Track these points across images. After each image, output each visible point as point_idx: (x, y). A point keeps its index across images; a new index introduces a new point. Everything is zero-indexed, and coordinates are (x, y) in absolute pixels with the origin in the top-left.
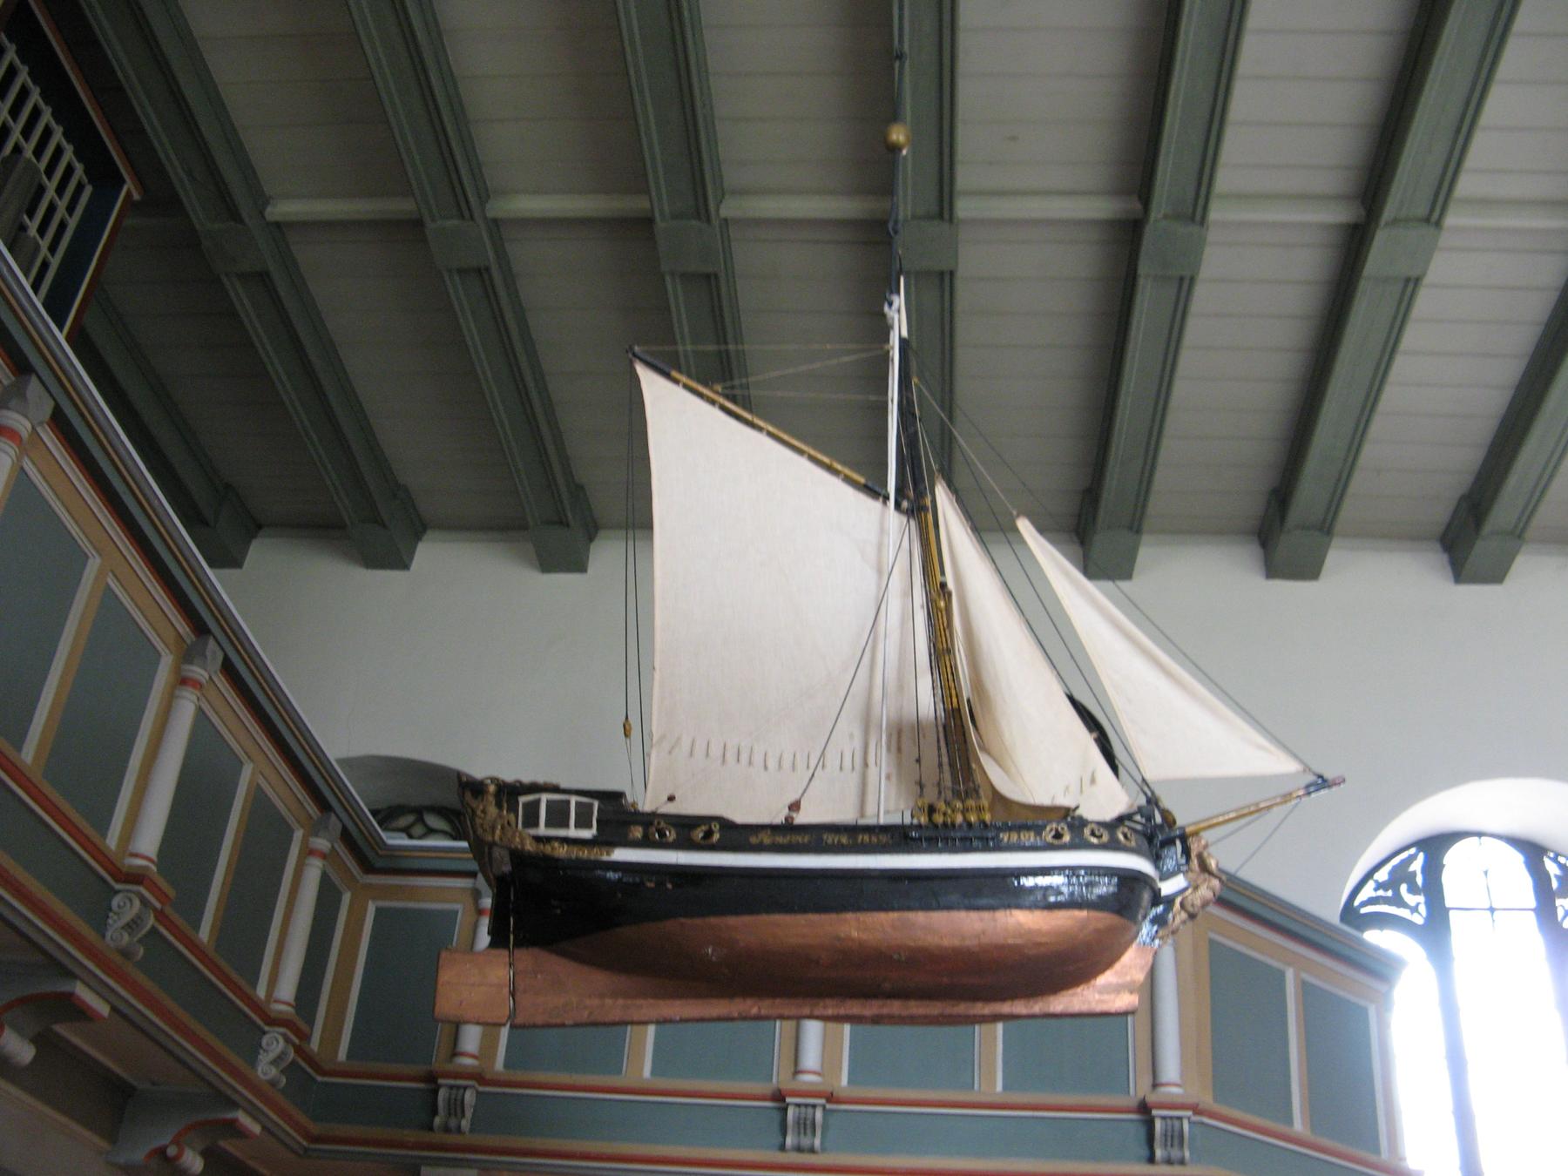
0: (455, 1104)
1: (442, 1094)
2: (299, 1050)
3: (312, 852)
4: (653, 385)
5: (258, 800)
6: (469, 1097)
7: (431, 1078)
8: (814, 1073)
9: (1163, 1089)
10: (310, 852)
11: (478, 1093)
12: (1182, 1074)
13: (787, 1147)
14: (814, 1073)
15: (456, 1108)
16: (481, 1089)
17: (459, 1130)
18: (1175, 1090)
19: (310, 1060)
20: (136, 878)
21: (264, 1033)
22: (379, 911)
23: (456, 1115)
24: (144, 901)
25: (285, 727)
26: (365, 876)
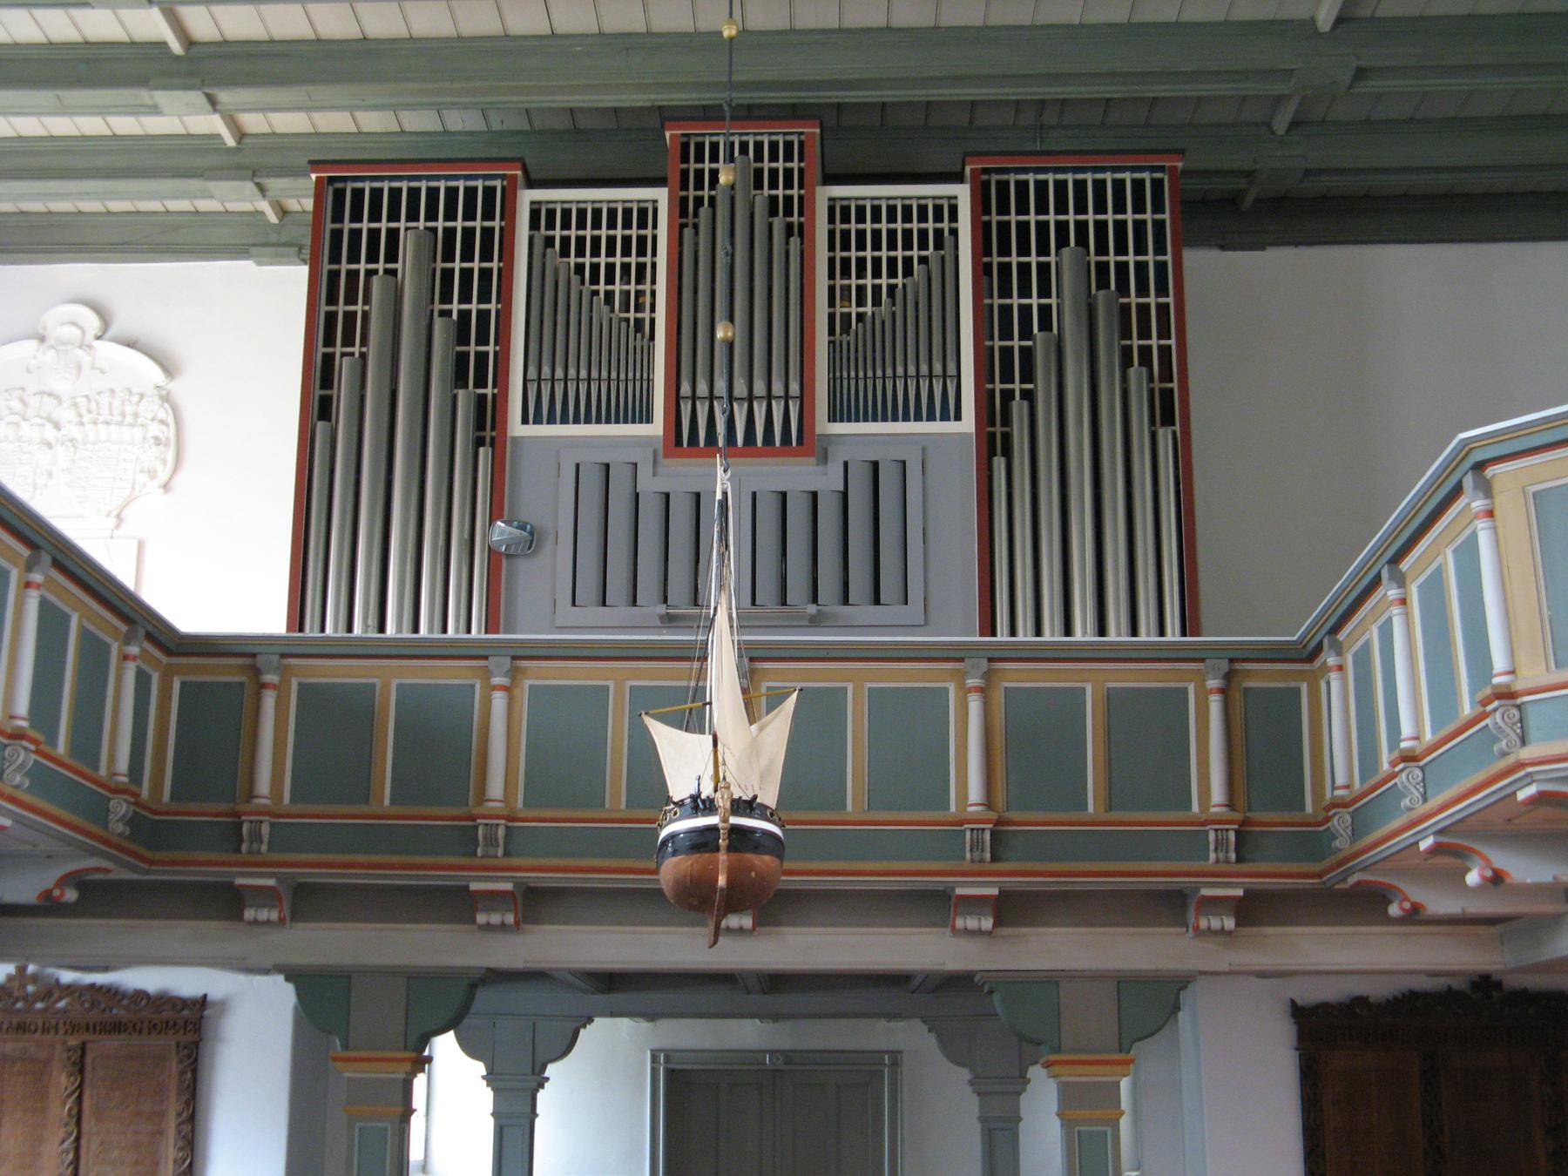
0: (255, 835)
1: (245, 829)
2: (137, 804)
3: (126, 657)
4: (445, 1047)
5: (84, 633)
6: (265, 829)
7: (237, 815)
8: (266, 798)
9: (257, 801)
10: (126, 657)
11: (1349, 813)
12: (1336, 796)
13: (508, 684)
14: (266, 798)
15: (256, 837)
16: (1350, 810)
17: (259, 852)
18: (263, 801)
19: (144, 807)
20: (18, 735)
21: (109, 800)
22: (183, 684)
23: (256, 840)
24: (26, 749)
25: (1383, 557)
26: (1314, 664)
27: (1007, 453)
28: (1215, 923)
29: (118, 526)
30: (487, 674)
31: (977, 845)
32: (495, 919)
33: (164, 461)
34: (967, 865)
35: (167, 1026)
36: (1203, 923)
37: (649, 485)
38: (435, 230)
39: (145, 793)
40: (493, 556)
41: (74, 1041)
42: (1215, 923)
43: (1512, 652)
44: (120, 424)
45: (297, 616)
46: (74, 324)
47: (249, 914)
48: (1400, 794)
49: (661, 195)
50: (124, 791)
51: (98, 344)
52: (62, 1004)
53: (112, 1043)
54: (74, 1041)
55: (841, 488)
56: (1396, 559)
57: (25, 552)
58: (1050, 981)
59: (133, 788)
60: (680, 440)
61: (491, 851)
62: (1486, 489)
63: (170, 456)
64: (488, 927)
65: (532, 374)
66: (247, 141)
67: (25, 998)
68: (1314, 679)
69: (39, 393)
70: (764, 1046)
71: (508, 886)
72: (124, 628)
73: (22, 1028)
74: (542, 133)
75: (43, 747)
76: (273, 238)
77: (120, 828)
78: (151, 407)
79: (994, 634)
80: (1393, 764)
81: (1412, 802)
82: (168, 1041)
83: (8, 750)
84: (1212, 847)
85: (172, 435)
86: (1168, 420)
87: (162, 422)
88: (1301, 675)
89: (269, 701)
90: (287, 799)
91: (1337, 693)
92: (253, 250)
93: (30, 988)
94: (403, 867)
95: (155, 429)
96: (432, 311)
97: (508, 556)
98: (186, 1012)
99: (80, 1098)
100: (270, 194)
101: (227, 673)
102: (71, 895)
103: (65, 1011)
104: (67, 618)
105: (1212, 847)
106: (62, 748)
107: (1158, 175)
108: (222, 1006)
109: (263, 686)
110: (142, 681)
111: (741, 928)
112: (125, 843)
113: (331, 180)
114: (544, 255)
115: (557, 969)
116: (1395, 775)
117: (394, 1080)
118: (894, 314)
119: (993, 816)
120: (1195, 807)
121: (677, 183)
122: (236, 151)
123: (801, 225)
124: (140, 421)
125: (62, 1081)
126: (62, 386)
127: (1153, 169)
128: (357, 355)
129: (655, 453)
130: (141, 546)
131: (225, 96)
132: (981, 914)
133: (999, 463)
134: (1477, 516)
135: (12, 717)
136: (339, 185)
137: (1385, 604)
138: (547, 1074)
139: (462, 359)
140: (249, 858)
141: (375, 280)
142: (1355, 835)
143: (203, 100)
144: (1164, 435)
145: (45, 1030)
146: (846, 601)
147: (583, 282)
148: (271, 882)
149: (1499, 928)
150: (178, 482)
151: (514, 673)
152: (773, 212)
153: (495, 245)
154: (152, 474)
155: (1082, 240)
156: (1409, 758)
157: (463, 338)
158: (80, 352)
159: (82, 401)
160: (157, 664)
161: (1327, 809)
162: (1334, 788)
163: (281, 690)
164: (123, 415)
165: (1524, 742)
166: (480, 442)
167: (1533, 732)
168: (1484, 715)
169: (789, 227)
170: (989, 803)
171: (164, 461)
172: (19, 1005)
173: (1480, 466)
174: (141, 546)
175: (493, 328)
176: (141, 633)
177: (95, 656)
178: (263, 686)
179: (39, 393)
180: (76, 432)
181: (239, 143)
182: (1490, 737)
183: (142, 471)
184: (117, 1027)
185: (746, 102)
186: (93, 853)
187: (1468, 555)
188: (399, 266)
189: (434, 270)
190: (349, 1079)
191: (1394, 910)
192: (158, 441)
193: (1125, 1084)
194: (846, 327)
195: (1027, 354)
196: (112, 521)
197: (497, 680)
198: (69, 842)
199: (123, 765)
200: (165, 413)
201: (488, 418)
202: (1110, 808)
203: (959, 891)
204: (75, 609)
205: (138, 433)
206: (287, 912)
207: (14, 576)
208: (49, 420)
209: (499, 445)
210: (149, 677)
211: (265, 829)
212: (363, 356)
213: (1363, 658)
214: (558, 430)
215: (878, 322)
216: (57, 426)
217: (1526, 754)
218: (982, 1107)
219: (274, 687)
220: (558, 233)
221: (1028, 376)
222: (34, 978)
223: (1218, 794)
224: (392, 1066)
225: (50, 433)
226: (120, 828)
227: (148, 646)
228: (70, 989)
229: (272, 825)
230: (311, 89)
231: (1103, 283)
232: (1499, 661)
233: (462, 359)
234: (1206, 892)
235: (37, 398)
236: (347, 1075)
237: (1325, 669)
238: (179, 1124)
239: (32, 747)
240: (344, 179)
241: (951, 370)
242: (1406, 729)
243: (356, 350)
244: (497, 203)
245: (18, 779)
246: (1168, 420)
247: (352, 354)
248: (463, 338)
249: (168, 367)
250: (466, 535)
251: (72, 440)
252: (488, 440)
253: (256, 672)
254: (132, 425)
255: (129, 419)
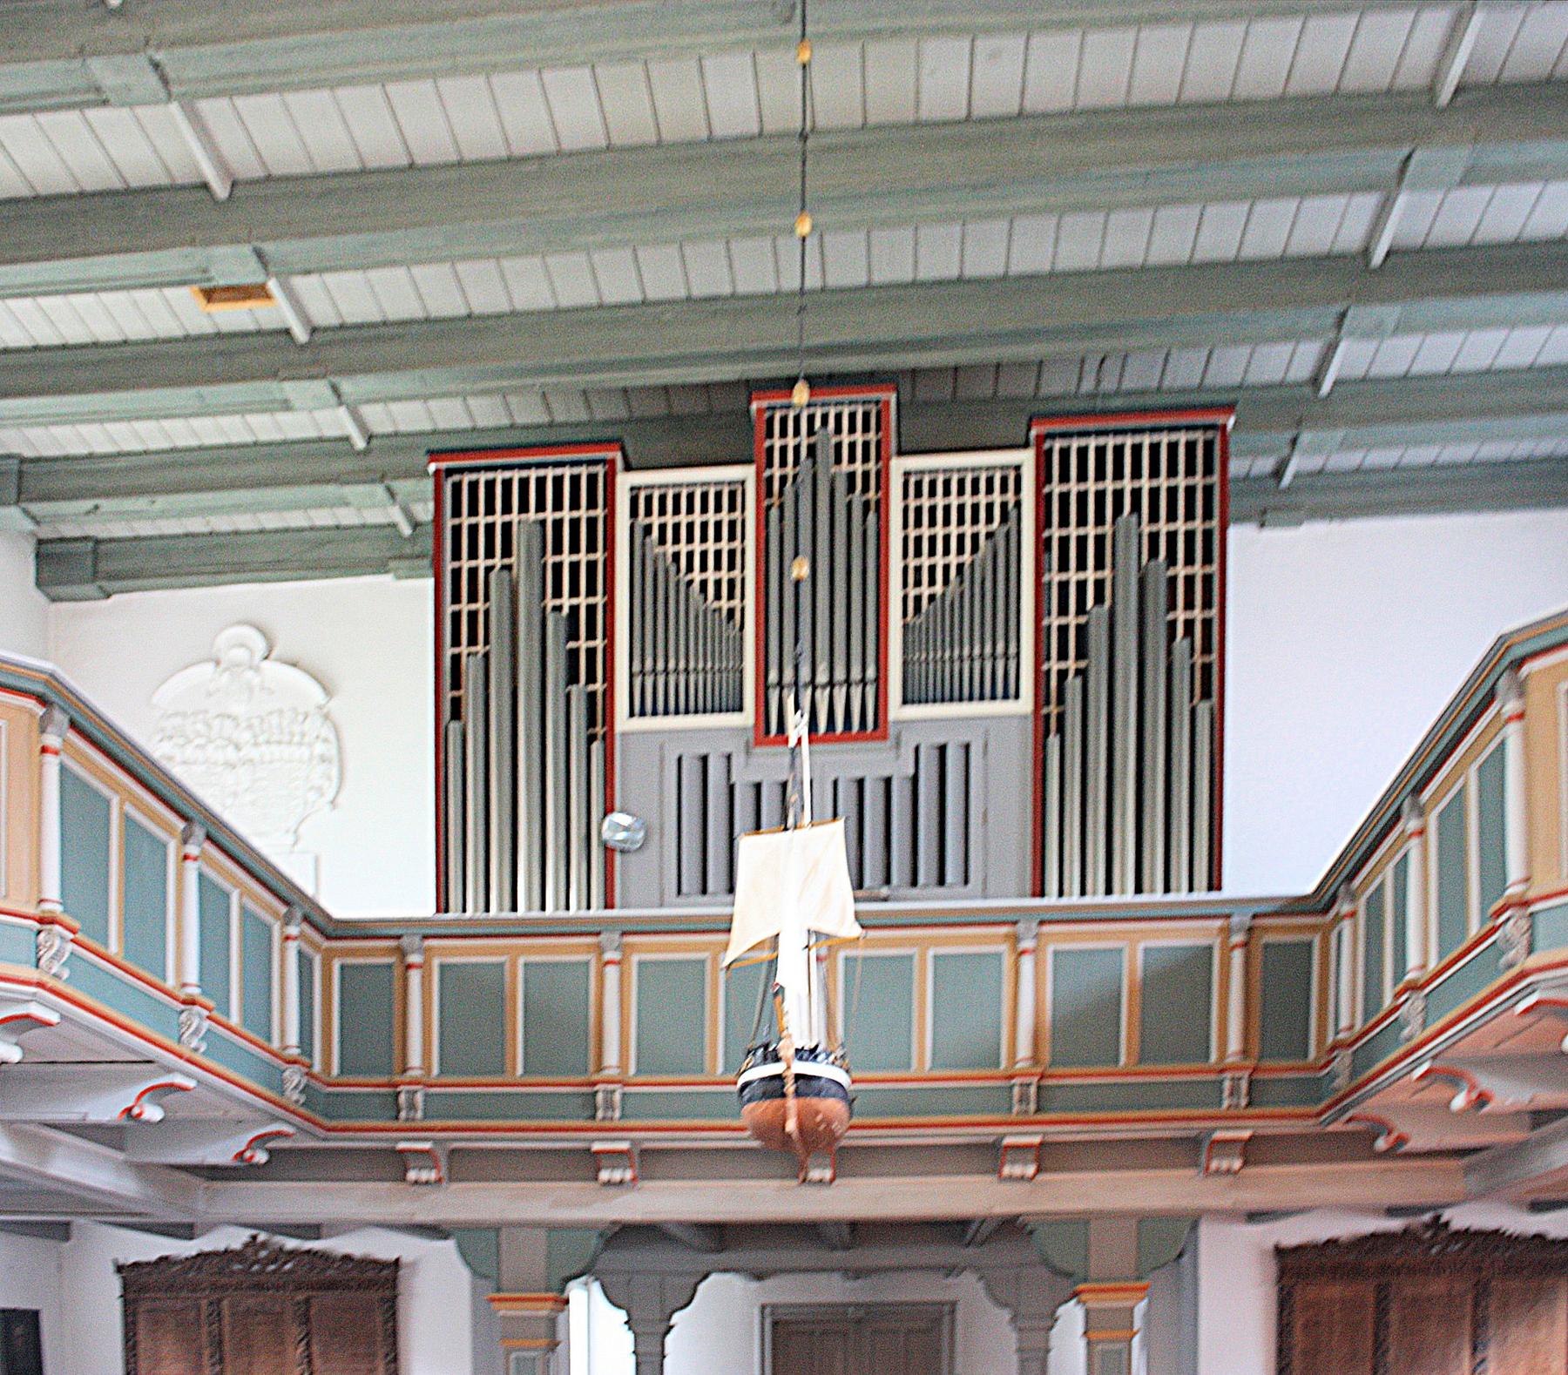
5: (243, 910)
6: (419, 1098)
24: (200, 1015)
27: (1061, 730)
28: (1224, 1164)
29: (295, 843)
30: (600, 950)
31: (1024, 1099)
32: (617, 1175)
33: (329, 778)
34: (1013, 1117)
35: (370, 1284)
36: (1214, 1165)
37: (743, 778)
38: (543, 523)
39: (317, 1068)
40: (608, 851)
41: (300, 1297)
42: (1224, 1164)
43: (1529, 861)
44: (290, 743)
45: (443, 905)
46: (242, 645)
47: (412, 1175)
48: (1399, 1025)
49: (747, 473)
50: (295, 1062)
51: (266, 664)
52: (288, 1266)
53: (330, 1297)
54: (300, 1297)
55: (911, 771)
56: (1418, 789)
57: (181, 825)
58: (1082, 1220)
59: (306, 1060)
60: (769, 731)
61: (609, 1114)
62: (1521, 691)
63: (334, 772)
64: (609, 1183)
65: (637, 667)
66: (374, 442)
67: (257, 1262)
68: (1325, 931)
69: (218, 716)
70: (845, 1300)
71: (624, 1146)
72: (283, 909)
73: (259, 1287)
74: (641, 420)
75: (215, 1014)
76: (408, 550)
77: (295, 1096)
78: (315, 726)
79: (1042, 894)
80: (1397, 996)
81: (1413, 1030)
82: (375, 1295)
83: (184, 1015)
84: (1226, 1093)
85: (334, 751)
86: (1206, 695)
87: (326, 740)
88: (1313, 928)
89: (415, 977)
90: (435, 1070)
91: (1350, 938)
92: (392, 564)
93: (263, 1254)
94: (536, 1130)
95: (319, 748)
96: (544, 608)
97: (623, 852)
98: (385, 1272)
99: (308, 1345)
100: (399, 498)
101: (375, 955)
102: (261, 1157)
103: (290, 1272)
104: (227, 896)
105: (1226, 1093)
106: (235, 1020)
107: (1210, 435)
108: (413, 1265)
109: (409, 967)
110: (304, 962)
111: (821, 1181)
112: (302, 1110)
113: (450, 472)
114: (643, 545)
115: (666, 1222)
116: (1397, 1008)
117: (537, 1318)
118: (962, 595)
119: (1039, 1070)
120: (1214, 1057)
121: (764, 461)
122: (366, 452)
123: (878, 502)
124: (306, 740)
125: (295, 1331)
126: (238, 709)
127: (1206, 428)
128: (480, 655)
129: (747, 743)
130: (317, 860)
131: (346, 386)
132: (1025, 1163)
133: (1053, 741)
134: (1510, 719)
135: (184, 985)
136: (456, 478)
137: (1405, 837)
138: (672, 1322)
139: (573, 655)
140: (408, 1125)
141: (493, 575)
142: (1354, 1073)
143: (328, 392)
144: (1203, 709)
145: (278, 1288)
146: (914, 883)
147: (678, 571)
148: (427, 1146)
149: (1466, 1160)
150: (340, 799)
151: (625, 949)
152: (851, 488)
153: (600, 535)
154: (320, 791)
155: (1136, 507)
156: (1414, 987)
157: (573, 635)
158: (249, 674)
159: (256, 722)
160: (317, 948)
161: (1333, 1049)
162: (1337, 1033)
163: (424, 967)
164: (292, 734)
165: (1530, 950)
166: (591, 739)
167: (1540, 942)
168: (1494, 930)
169: (866, 505)
170: (1035, 1058)
171: (329, 778)
172: (256, 1267)
173: (1519, 663)
174: (317, 860)
175: (599, 621)
176: (299, 914)
177: (258, 938)
178: (409, 967)
179: (218, 716)
180: (255, 753)
181: (368, 443)
182: (1498, 950)
183: (312, 788)
184: (331, 1285)
185: (827, 371)
186: (275, 1119)
187: (1495, 767)
188: (513, 560)
189: (544, 566)
190: (503, 1317)
191: (1381, 1144)
192: (323, 759)
193: (1140, 1308)
194: (918, 609)
195: (1082, 630)
196: (290, 838)
197: (608, 956)
198: (257, 1109)
199: (293, 1038)
200: (327, 732)
201: (599, 712)
202: (1141, 1061)
203: (1008, 1141)
204: (236, 886)
205: (305, 751)
206: (444, 1172)
207: (172, 846)
208: (230, 740)
209: (608, 739)
210: (311, 962)
211: (419, 1098)
212: (486, 656)
213: (1376, 901)
214: (661, 722)
215: (948, 603)
216: (238, 747)
217: (1532, 962)
218: (1020, 1340)
219: (420, 966)
220: (656, 520)
221: (1082, 653)
222: (264, 1245)
223: (1234, 1044)
224: (539, 1305)
225: (231, 754)
226: (295, 1096)
227: (306, 928)
228: (293, 1253)
229: (426, 1095)
230: (426, 373)
231: (1154, 553)
232: (1515, 871)
233: (573, 655)
234: (1218, 1135)
235: (217, 722)
236: (501, 1313)
237: (1338, 918)
238: (387, 1364)
239: (206, 1013)
240: (461, 471)
241: (1012, 650)
242: (1413, 959)
243: (480, 648)
244: (600, 491)
245: (194, 1043)
246: (1206, 695)
247: (476, 653)
248: (573, 635)
249: (328, 691)
250: (584, 831)
251: (251, 761)
252: (600, 737)
253: (402, 953)
254: (300, 744)
255: (296, 739)
